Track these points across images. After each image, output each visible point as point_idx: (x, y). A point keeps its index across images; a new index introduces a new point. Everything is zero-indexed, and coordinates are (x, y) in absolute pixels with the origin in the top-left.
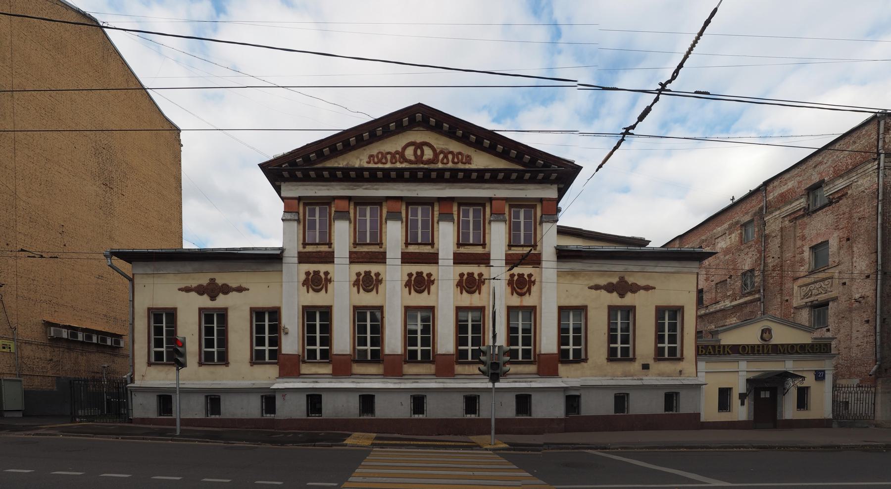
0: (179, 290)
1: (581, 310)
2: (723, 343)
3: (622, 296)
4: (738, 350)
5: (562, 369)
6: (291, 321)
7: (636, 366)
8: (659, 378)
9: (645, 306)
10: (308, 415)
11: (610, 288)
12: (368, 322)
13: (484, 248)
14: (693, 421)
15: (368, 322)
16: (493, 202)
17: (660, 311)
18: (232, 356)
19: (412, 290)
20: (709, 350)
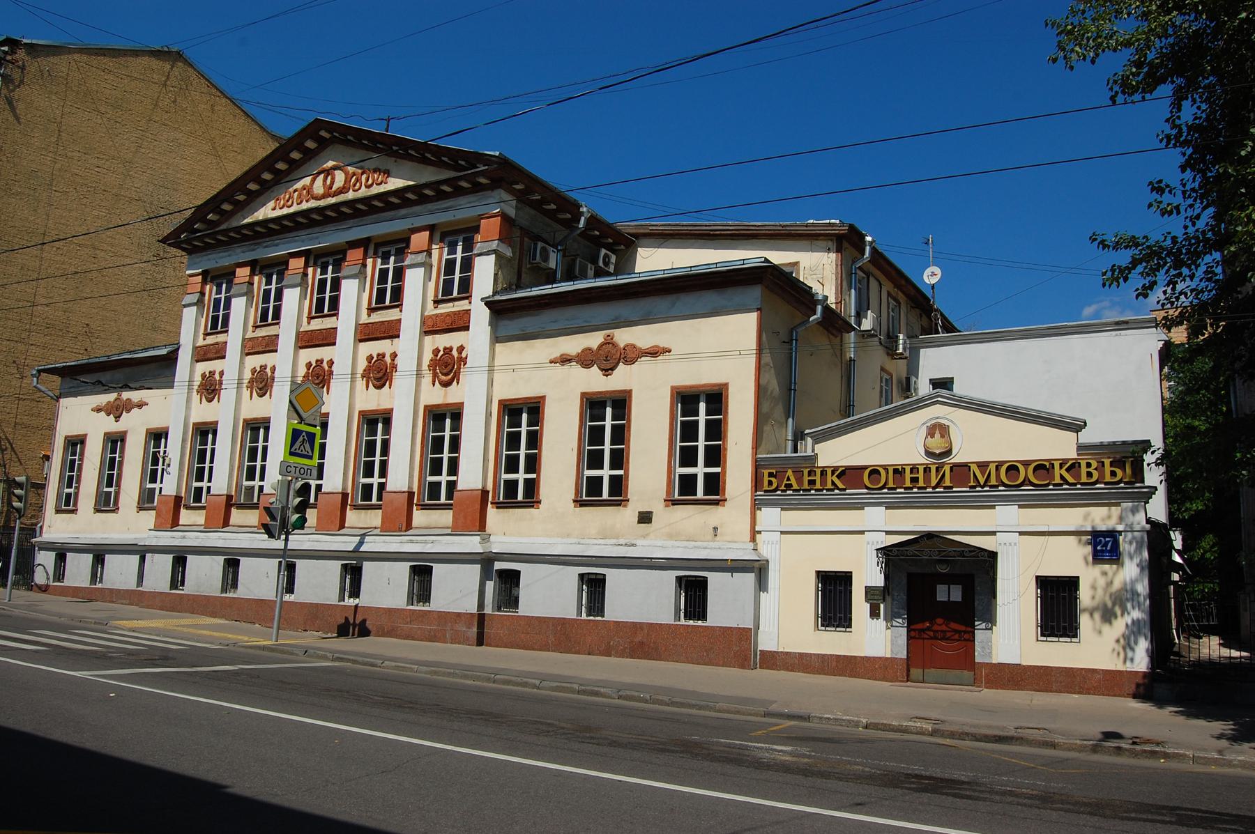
0: (551, 362)
1: (535, 408)
2: (821, 463)
3: (607, 371)
4: (858, 482)
7: (625, 516)
8: (670, 543)
9: (651, 394)
10: (410, 602)
14: (738, 647)
17: (686, 399)
18: (544, 491)
19: (255, 393)
20: (784, 481)
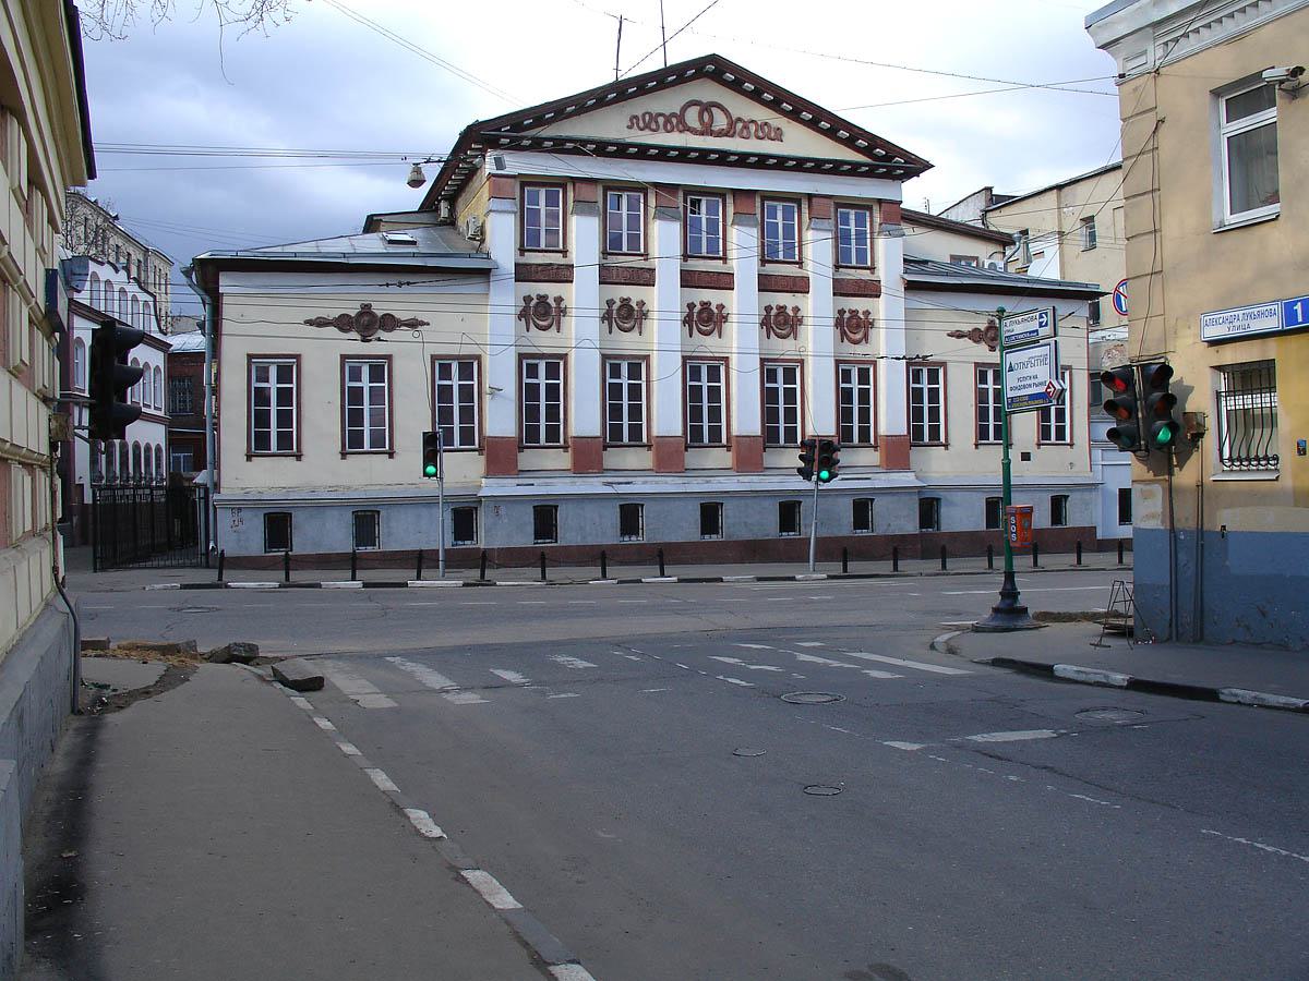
0: (949, 335)
3: (366, 310)
5: (844, 457)
6: (500, 374)
10: (265, 552)
11: (343, 323)
12: (624, 385)
13: (801, 268)
15: (624, 385)
16: (814, 200)
